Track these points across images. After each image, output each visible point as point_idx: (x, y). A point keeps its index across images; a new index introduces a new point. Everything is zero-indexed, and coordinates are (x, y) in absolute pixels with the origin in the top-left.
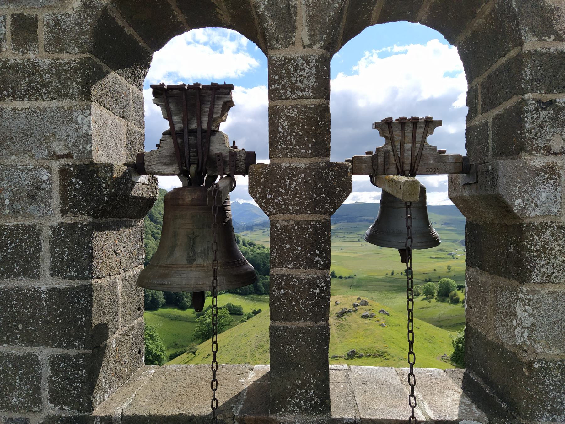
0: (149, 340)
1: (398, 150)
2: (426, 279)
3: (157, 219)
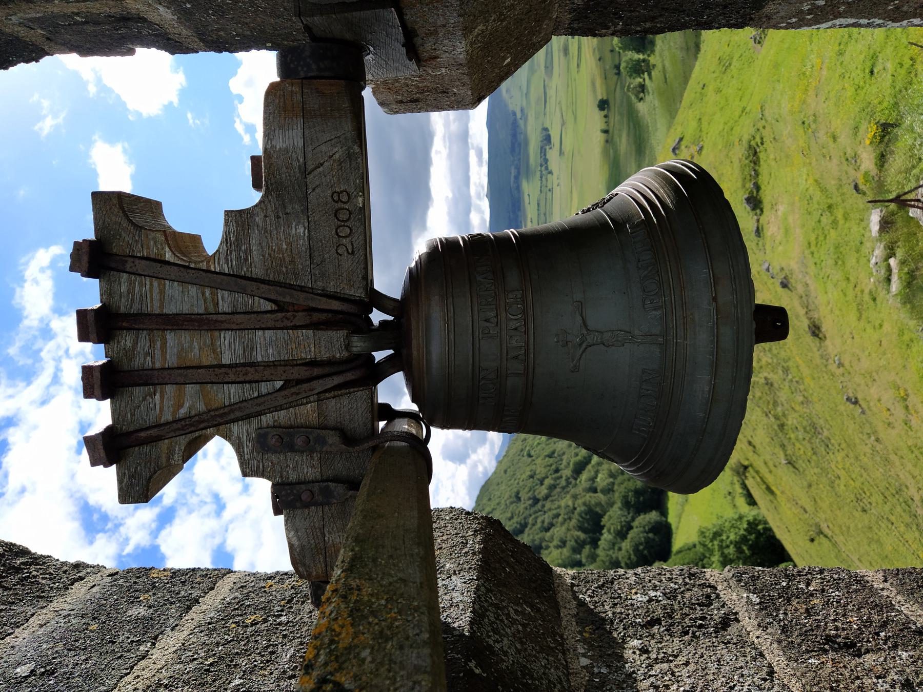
0: (722, 541)
1: (250, 391)
2: (616, 74)
3: (520, 524)
